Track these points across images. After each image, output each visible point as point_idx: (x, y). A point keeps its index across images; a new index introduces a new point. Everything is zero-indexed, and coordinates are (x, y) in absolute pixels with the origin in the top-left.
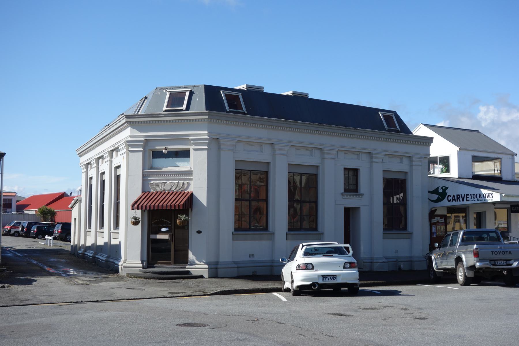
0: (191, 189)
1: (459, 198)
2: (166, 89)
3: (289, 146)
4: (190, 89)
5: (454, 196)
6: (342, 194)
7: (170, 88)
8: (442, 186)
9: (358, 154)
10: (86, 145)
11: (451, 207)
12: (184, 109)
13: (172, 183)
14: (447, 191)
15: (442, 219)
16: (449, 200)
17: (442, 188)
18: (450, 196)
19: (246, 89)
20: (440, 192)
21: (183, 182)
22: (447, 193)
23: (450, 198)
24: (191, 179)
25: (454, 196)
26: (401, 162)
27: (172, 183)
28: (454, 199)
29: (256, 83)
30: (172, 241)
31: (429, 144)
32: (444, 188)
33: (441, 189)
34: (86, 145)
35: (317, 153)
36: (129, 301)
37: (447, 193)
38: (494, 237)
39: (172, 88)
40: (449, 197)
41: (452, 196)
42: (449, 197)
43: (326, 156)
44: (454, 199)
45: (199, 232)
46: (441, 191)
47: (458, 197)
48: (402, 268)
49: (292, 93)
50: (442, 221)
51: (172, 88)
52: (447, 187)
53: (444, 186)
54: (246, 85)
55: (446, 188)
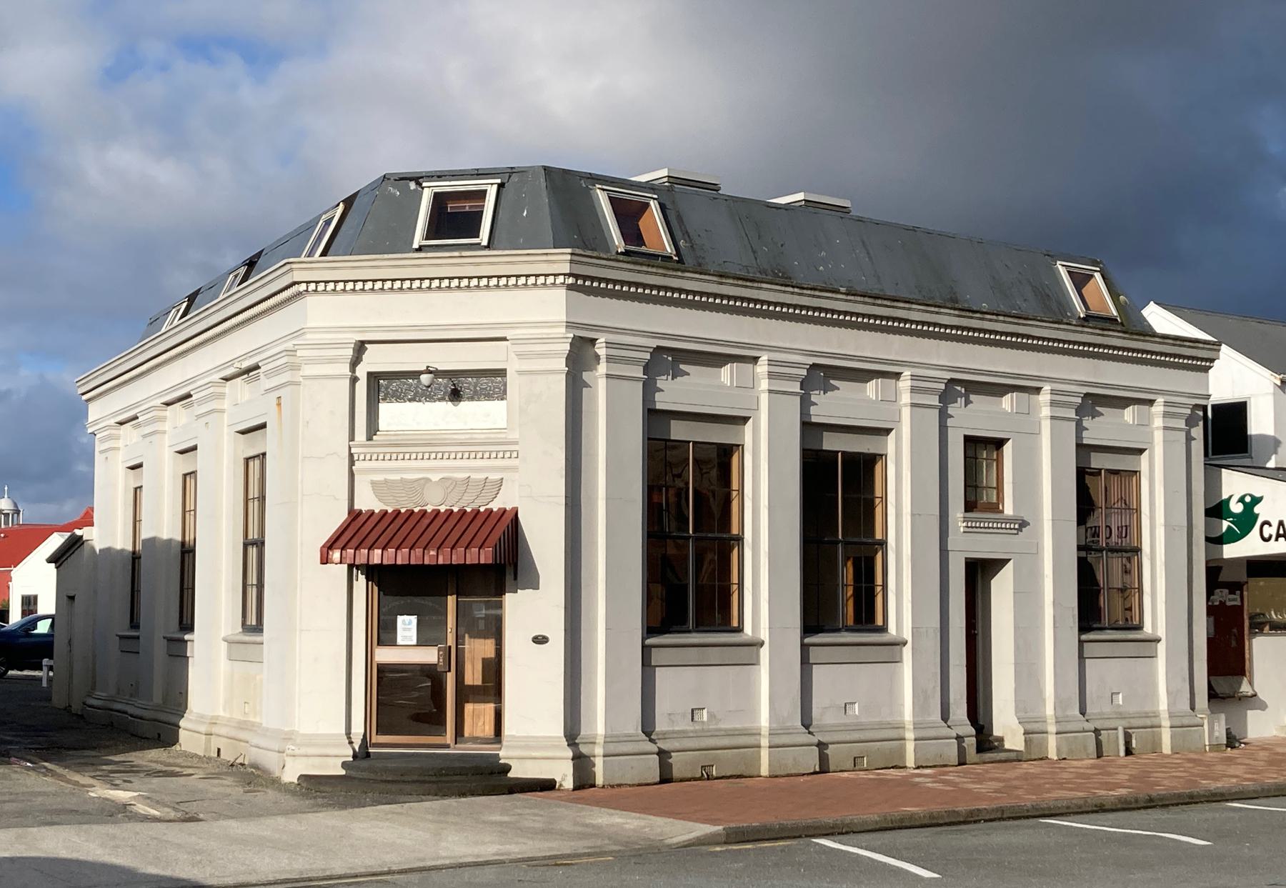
2: (418, 179)
4: (499, 181)
7: (440, 176)
10: (120, 364)
11: (1270, 559)
12: (485, 243)
13: (450, 482)
14: (1257, 510)
15: (1235, 594)
16: (1266, 535)
17: (1242, 500)
18: (1270, 525)
19: (666, 184)
22: (1258, 514)
23: (1267, 531)
24: (514, 469)
27: (450, 482)
30: (450, 671)
32: (1248, 499)
34: (120, 364)
36: (386, 882)
37: (1258, 514)
38: (1231, 644)
39: (439, 177)
40: (1266, 527)
41: (1275, 525)
42: (1266, 527)
45: (540, 640)
50: (1234, 600)
51: (439, 177)
53: (1250, 495)
55: (1256, 500)
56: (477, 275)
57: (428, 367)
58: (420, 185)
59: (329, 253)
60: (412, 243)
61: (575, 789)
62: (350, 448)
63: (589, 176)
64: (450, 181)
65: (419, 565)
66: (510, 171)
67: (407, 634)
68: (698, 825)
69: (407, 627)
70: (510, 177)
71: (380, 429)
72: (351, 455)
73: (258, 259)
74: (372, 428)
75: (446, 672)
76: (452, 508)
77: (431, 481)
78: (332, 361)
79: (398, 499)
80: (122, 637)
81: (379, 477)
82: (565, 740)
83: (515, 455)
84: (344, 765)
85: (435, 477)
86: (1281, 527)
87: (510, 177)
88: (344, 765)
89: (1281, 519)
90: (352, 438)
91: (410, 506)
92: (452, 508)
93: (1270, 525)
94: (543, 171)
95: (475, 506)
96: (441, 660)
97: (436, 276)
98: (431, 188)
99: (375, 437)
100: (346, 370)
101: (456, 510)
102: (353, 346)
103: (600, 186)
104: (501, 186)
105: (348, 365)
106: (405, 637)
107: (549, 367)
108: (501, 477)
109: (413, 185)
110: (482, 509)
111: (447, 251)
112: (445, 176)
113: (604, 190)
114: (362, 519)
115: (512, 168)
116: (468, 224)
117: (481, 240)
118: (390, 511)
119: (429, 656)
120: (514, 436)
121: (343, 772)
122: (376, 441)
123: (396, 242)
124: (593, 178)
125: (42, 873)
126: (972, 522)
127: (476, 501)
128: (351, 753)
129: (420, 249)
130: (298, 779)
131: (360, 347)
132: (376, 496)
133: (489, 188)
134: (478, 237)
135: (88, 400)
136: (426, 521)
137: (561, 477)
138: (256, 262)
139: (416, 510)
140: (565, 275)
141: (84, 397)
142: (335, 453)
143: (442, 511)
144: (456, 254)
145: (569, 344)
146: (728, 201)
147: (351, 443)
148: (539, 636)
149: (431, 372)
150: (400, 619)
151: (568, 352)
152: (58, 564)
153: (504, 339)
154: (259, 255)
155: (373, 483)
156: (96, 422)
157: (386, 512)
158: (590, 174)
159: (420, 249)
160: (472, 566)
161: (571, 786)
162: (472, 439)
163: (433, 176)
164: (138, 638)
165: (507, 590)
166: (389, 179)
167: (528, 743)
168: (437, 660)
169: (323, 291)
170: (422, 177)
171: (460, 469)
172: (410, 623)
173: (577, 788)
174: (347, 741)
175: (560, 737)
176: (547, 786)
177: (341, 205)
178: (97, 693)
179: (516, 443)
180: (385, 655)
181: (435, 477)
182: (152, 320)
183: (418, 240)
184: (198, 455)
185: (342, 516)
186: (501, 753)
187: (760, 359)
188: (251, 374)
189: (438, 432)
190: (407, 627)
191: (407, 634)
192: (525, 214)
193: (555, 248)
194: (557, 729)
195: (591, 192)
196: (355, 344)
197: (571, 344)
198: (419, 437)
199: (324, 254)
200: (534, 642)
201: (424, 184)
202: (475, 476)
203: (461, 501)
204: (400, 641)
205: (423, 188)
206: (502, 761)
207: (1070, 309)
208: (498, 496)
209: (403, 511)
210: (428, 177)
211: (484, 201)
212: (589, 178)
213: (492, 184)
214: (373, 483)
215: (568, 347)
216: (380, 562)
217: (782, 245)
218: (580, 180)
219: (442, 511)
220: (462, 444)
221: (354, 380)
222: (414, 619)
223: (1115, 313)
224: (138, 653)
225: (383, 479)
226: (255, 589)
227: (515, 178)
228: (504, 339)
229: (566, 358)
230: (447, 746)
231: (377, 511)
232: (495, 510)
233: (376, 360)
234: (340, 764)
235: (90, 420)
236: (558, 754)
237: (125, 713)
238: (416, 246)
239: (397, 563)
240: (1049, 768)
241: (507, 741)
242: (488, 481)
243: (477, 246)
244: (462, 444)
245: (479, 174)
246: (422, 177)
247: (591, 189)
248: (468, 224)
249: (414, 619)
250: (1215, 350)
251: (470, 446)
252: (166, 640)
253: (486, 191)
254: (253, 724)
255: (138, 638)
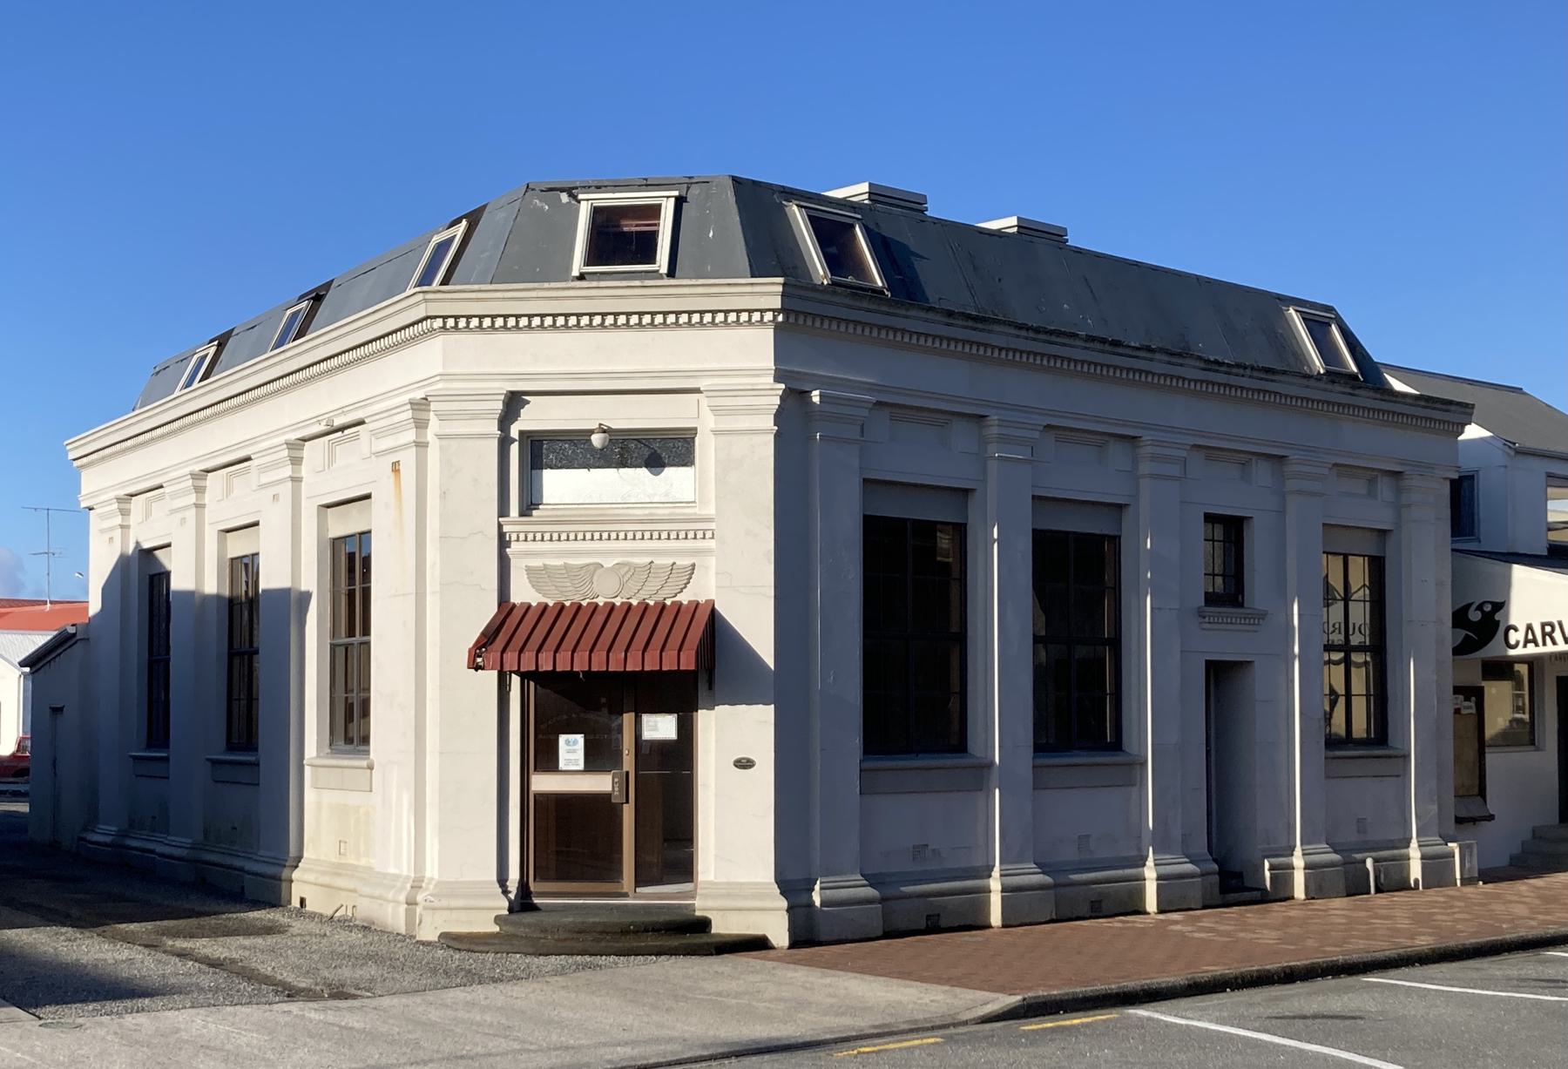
0: (702, 590)
1: (1550, 635)
3: (870, 406)
4: (676, 193)
5: (1529, 628)
6: (1201, 614)
8: (1482, 601)
9: (1245, 459)
12: (664, 270)
18: (1516, 630)
19: (866, 202)
20: (1480, 617)
21: (671, 562)
24: (708, 552)
25: (1529, 628)
26: (1372, 494)
27: (626, 569)
28: (1530, 637)
29: (902, 181)
30: (627, 802)
31: (1460, 430)
32: (1488, 608)
33: (1476, 610)
35: (1385, 488)
40: (1512, 631)
42: (1512, 631)
43: (1291, 485)
44: (1530, 637)
45: (744, 764)
46: (1475, 616)
47: (1548, 629)
48: (1382, 885)
49: (1016, 223)
52: (1503, 601)
54: (867, 184)
56: (700, 309)
57: (600, 424)
58: (575, 197)
59: (451, 281)
60: (569, 268)
61: (790, 948)
62: (500, 526)
63: (782, 190)
64: (614, 192)
65: (655, 671)
66: (687, 180)
67: (572, 756)
68: (1000, 996)
69: (571, 748)
70: (688, 188)
71: (544, 502)
72: (501, 535)
73: (327, 292)
74: (529, 506)
75: (622, 804)
76: (630, 600)
77: (603, 567)
78: (475, 416)
79: (560, 589)
80: (215, 763)
81: (537, 563)
82: (498, 886)
83: (709, 534)
84: (498, 919)
85: (609, 563)
86: (1530, 632)
87: (688, 188)
88: (498, 919)
89: (1529, 622)
90: (503, 511)
91: (577, 599)
92: (630, 600)
93: (1516, 630)
94: (730, 181)
95: (659, 598)
96: (616, 789)
97: (450, 314)
98: (590, 202)
99: (535, 513)
100: (493, 428)
101: (635, 602)
102: (503, 397)
103: (797, 202)
104: (680, 201)
105: (496, 421)
106: (569, 761)
107: (754, 426)
108: (691, 562)
109: (564, 197)
110: (668, 602)
111: (624, 279)
112: (606, 186)
113: (802, 207)
114: (517, 615)
115: (690, 178)
116: (644, 248)
117: (660, 266)
118: (551, 604)
119: (601, 783)
120: (711, 510)
121: (497, 929)
122: (537, 517)
123: (549, 268)
124: (786, 193)
125: (448, 1059)
126: (1214, 617)
127: (659, 592)
128: (506, 904)
129: (582, 277)
130: (439, 937)
131: (514, 403)
132: (533, 586)
133: (664, 202)
134: (655, 263)
135: (82, 467)
136: (599, 619)
137: (769, 562)
138: (324, 296)
139: (584, 603)
140: (773, 310)
141: (76, 464)
142: (480, 532)
143: (618, 604)
144: (637, 283)
145: (501, 402)
146: (937, 225)
147: (500, 519)
148: (744, 759)
149: (604, 432)
150: (563, 738)
151: (777, 407)
152: (34, 669)
153: (697, 391)
154: (328, 286)
155: (529, 570)
156: (93, 494)
157: (546, 606)
158: (783, 187)
159: (582, 277)
160: (563, 673)
161: (786, 943)
162: (651, 514)
163: (589, 187)
164: (167, 759)
165: (699, 706)
166: (533, 190)
167: (732, 890)
168: (611, 789)
169: (465, 328)
170: (577, 188)
171: (639, 552)
172: (575, 742)
173: (794, 944)
174: (500, 890)
175: (769, 884)
176: (758, 944)
177: (464, 222)
178: (101, 826)
179: (710, 520)
180: (543, 783)
181: (609, 563)
182: (157, 369)
183: (577, 266)
184: (261, 530)
185: (488, 610)
186: (698, 903)
187: (989, 418)
188: (346, 432)
189: (608, 506)
190: (571, 748)
191: (572, 756)
192: (711, 235)
193: (752, 277)
194: (492, 875)
195: (787, 209)
196: (506, 395)
197: (782, 398)
198: (583, 512)
199: (445, 282)
200: (736, 766)
201: (581, 196)
202: (659, 561)
203: (644, 588)
204: (562, 765)
205: (579, 202)
206: (698, 913)
207: (1307, 362)
208: (684, 590)
209: (568, 604)
210: (584, 187)
211: (659, 218)
212: (782, 192)
213: (668, 197)
214: (529, 570)
215: (777, 401)
216: (534, 669)
217: (1000, 280)
218: (773, 194)
219: (618, 604)
220: (641, 522)
221: (504, 443)
222: (579, 739)
223: (1354, 369)
224: (168, 778)
225: (541, 564)
226: (1344, 698)
227: (695, 190)
228: (697, 391)
229: (775, 415)
230: (625, 895)
231: (534, 604)
232: (685, 603)
233: (534, 418)
234: (494, 917)
235: (83, 492)
236: (768, 904)
237: (153, 852)
238: (575, 273)
239: (592, 670)
240: (1374, 924)
241: (701, 888)
242: (675, 567)
243: (655, 274)
244: (641, 522)
245: (648, 185)
246: (577, 188)
247: (786, 206)
248: (644, 248)
249: (579, 739)
250: (1465, 413)
251: (651, 526)
252: (209, 764)
253: (660, 205)
254: (355, 868)
255: (167, 759)
